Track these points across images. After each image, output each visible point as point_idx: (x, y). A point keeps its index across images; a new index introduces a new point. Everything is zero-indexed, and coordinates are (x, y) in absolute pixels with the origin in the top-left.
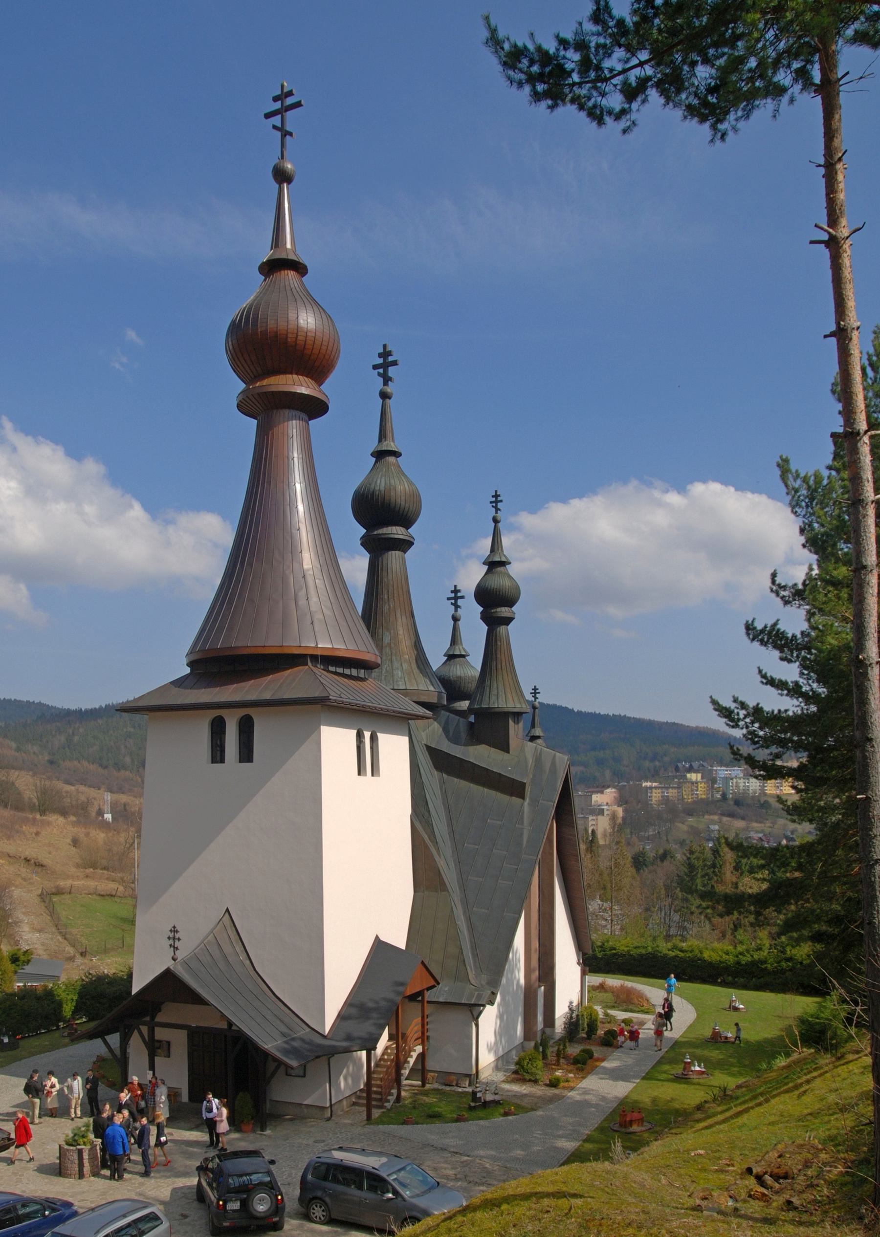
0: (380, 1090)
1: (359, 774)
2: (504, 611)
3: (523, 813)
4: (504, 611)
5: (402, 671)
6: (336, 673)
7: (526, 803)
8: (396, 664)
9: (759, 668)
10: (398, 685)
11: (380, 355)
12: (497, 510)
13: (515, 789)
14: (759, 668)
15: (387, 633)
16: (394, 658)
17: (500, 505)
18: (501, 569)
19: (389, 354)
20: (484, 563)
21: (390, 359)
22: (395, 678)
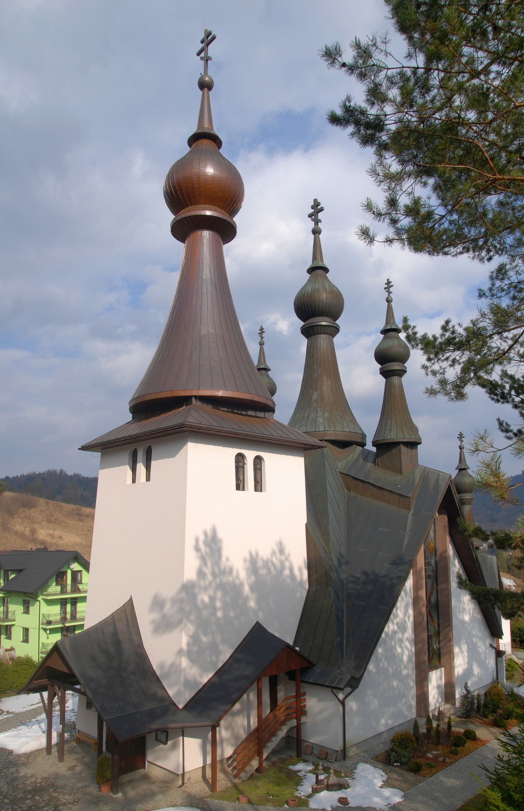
0: (68, 616)
1: (238, 488)
2: (395, 366)
3: (407, 521)
4: (395, 366)
5: (323, 419)
6: (237, 413)
7: (410, 514)
8: (319, 414)
9: (498, 420)
10: (319, 428)
11: (386, 284)
12: (389, 293)
13: (402, 499)
14: (498, 420)
15: (315, 392)
16: (319, 409)
17: (391, 289)
18: (464, 471)
19: (390, 282)
20: (456, 469)
21: (391, 284)
22: (318, 423)
